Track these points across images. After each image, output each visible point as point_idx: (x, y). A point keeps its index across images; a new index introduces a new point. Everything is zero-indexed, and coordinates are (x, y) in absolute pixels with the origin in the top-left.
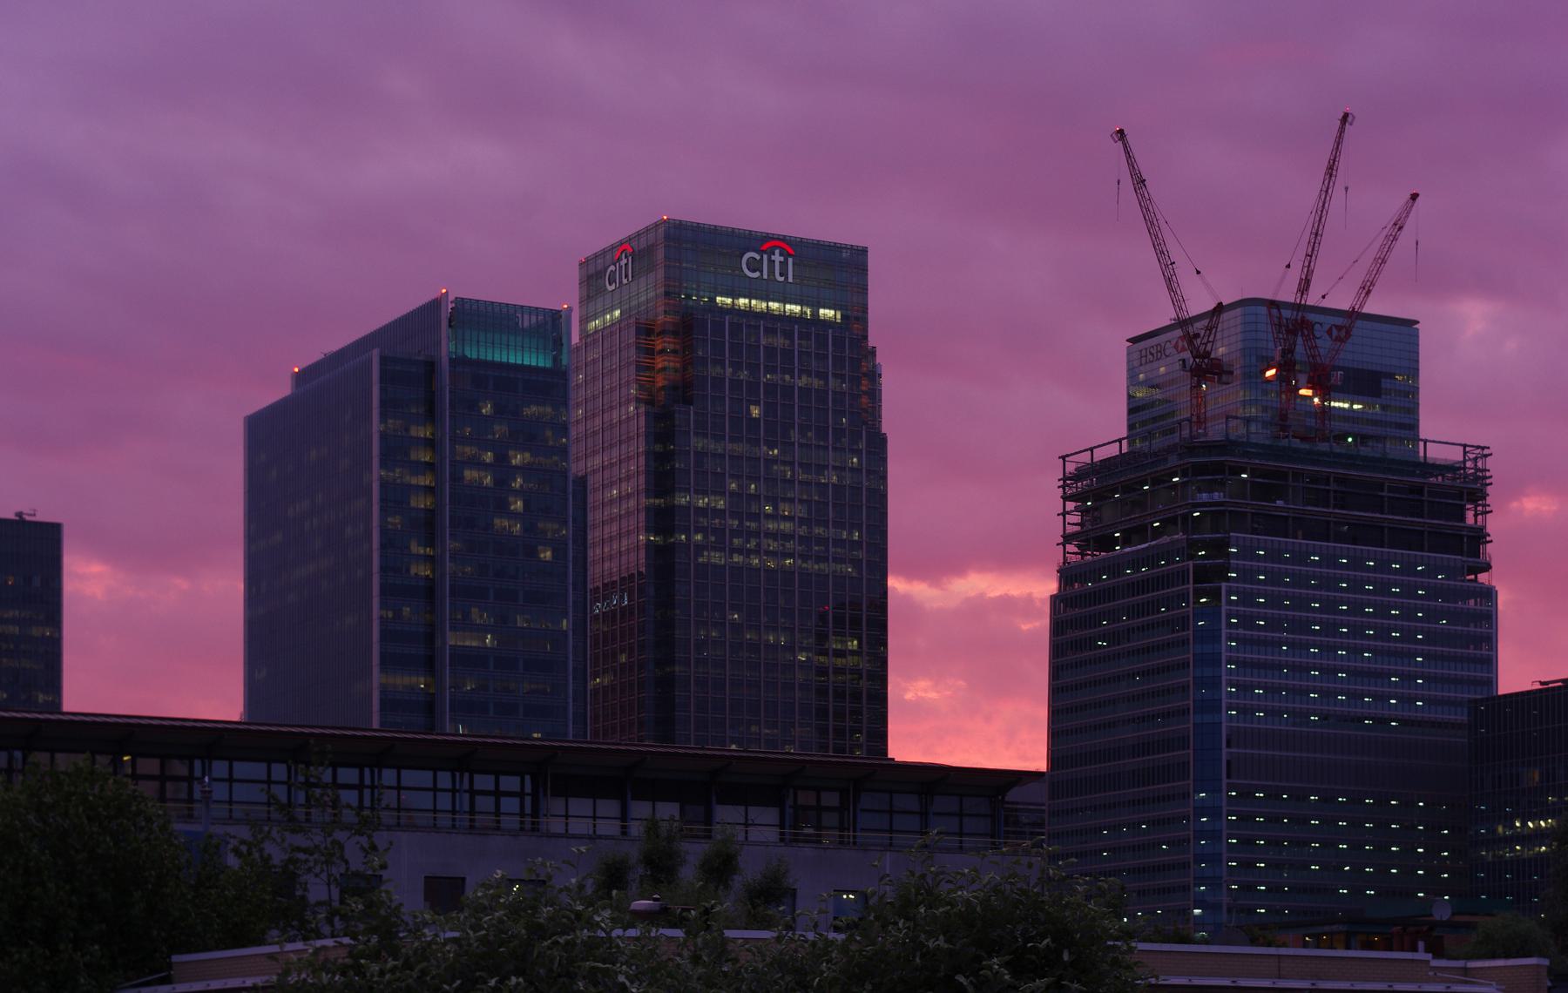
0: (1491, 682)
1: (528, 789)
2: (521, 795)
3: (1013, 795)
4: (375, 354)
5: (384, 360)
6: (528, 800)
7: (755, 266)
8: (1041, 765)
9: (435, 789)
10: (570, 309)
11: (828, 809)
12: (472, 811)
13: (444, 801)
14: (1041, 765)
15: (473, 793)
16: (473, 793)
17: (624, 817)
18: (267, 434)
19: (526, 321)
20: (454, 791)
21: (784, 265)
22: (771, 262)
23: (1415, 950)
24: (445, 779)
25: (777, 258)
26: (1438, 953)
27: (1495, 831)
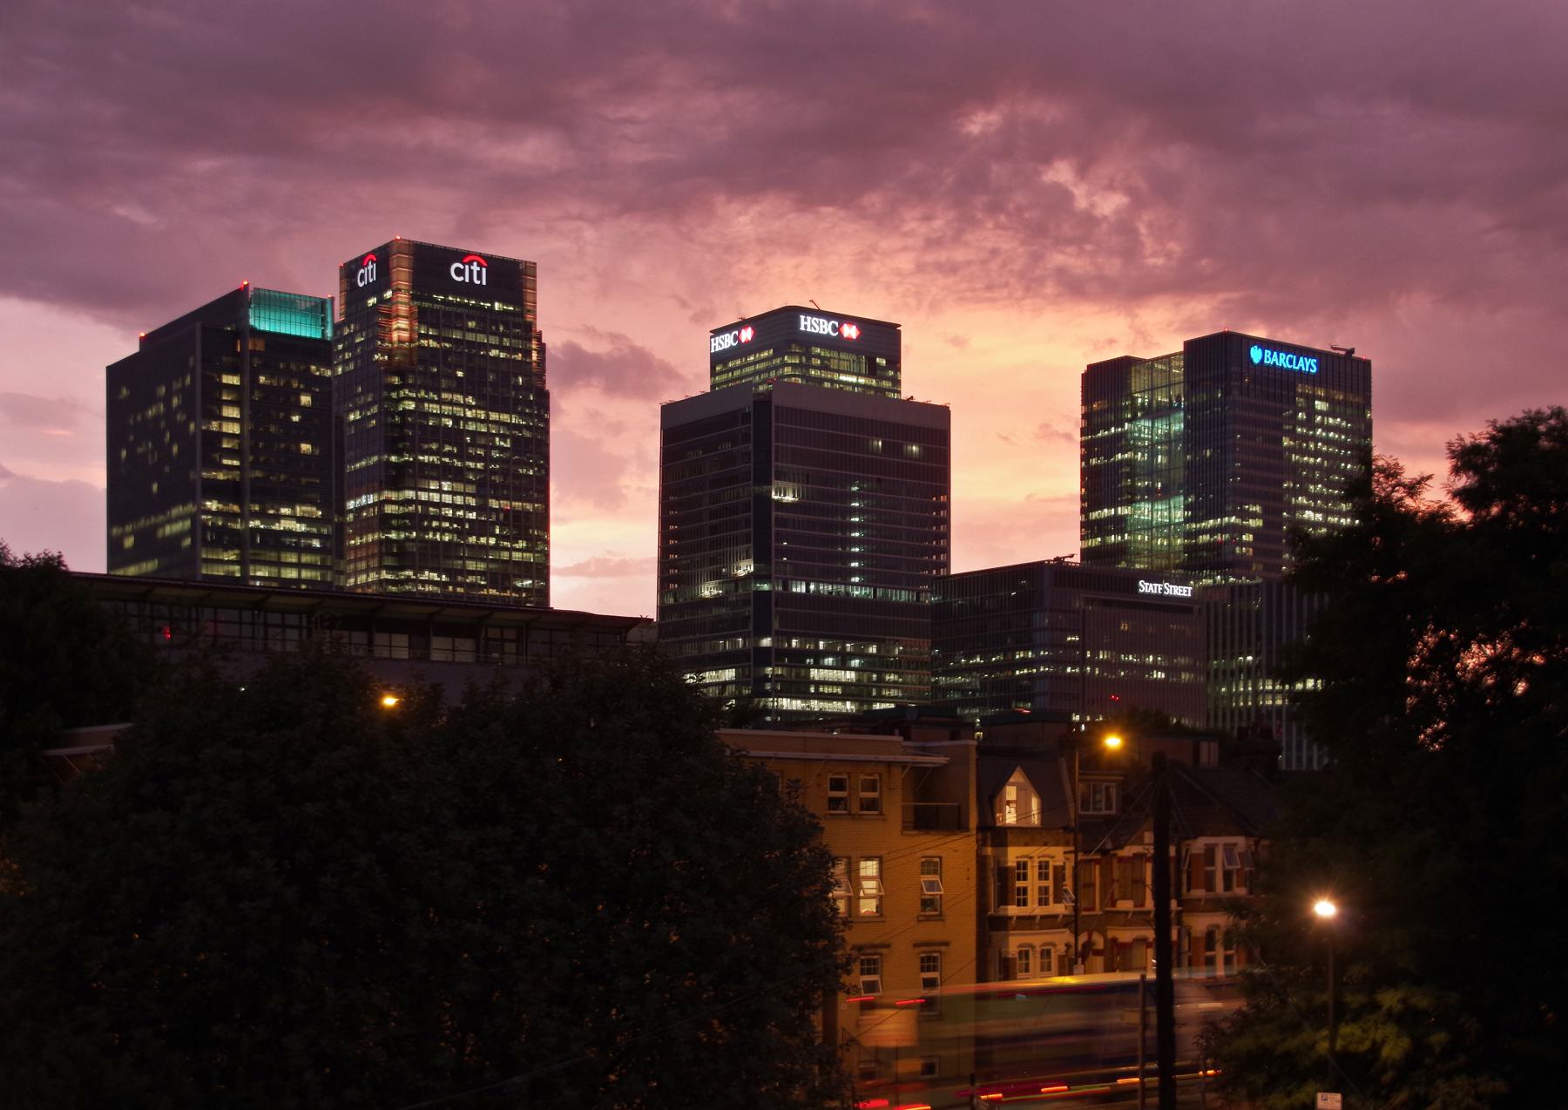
0: (947, 565)
1: (304, 623)
2: (299, 627)
3: (634, 634)
4: (198, 325)
5: (204, 329)
6: (305, 631)
7: (459, 272)
8: (652, 613)
9: (240, 623)
10: (333, 299)
11: (293, 627)
12: (266, 638)
13: (247, 631)
14: (652, 613)
15: (266, 625)
16: (266, 625)
17: (370, 642)
18: (1084, 376)
19: (1050, 289)
20: (253, 624)
21: (479, 273)
22: (471, 272)
23: (892, 734)
24: (247, 616)
25: (475, 268)
26: (907, 738)
27: (1489, 688)
